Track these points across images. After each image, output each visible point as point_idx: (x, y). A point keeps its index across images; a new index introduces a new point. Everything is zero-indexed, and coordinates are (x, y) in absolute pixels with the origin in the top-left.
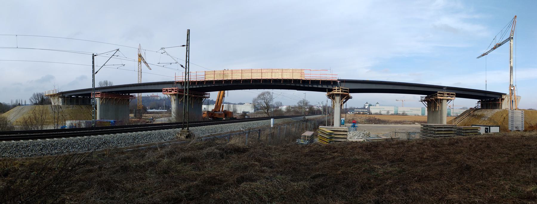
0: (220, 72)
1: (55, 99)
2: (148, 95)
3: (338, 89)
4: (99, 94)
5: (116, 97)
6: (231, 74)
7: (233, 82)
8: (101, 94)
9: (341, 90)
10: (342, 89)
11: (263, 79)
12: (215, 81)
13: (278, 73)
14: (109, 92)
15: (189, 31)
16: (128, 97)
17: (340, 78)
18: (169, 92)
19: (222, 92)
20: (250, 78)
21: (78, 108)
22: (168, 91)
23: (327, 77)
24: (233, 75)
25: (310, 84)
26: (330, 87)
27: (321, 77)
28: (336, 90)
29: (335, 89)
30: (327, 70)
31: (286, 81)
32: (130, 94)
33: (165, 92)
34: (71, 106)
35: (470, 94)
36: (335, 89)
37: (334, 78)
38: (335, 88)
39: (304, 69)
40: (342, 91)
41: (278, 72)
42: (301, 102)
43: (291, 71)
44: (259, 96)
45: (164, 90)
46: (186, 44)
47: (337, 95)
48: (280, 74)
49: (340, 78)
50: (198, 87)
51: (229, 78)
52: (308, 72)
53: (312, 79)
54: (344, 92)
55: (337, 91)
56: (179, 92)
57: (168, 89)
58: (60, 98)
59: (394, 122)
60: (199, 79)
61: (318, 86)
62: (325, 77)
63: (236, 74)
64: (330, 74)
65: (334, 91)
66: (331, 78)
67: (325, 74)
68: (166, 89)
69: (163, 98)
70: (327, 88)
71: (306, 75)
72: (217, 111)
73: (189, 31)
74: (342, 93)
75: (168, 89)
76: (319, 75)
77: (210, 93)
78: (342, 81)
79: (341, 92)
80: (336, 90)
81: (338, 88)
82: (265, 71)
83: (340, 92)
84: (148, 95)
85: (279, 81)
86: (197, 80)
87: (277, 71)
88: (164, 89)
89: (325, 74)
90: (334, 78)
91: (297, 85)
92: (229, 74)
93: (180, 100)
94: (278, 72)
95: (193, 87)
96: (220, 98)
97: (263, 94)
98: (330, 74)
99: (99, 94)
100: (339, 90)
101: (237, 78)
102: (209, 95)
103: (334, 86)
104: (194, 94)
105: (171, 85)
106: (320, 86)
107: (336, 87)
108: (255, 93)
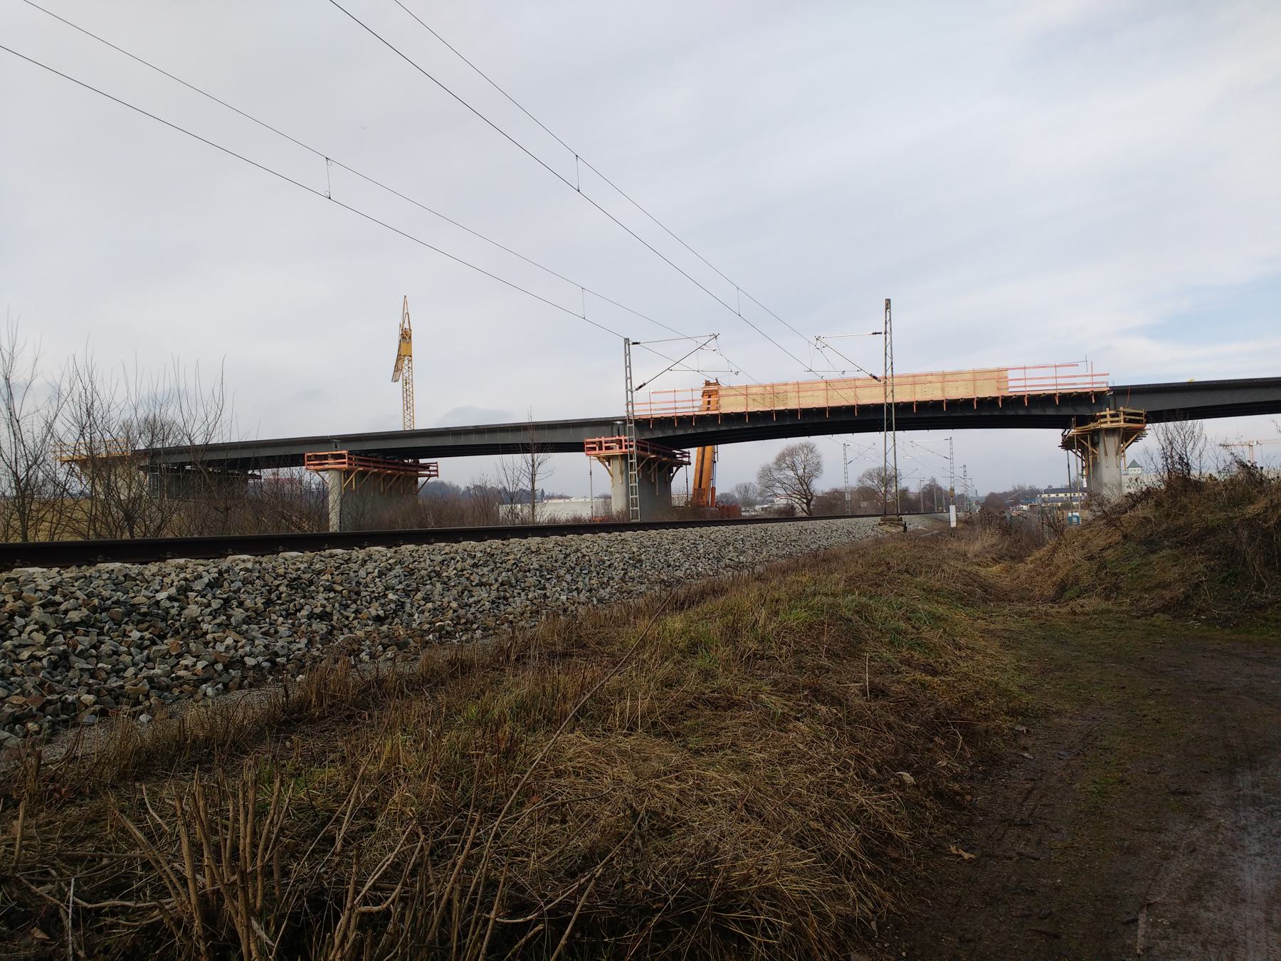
0: (760, 390)
3: (1112, 416)
9: (1122, 417)
10: (1125, 413)
11: (655, 418)
12: (750, 414)
13: (930, 385)
16: (415, 469)
19: (708, 448)
20: (852, 402)
22: (604, 445)
23: (1075, 384)
26: (1083, 411)
27: (1056, 385)
29: (1105, 416)
31: (953, 404)
32: (422, 461)
33: (594, 449)
36: (1105, 416)
37: (1095, 383)
38: (1102, 413)
40: (1125, 421)
41: (930, 382)
42: (870, 476)
43: (968, 376)
44: (781, 458)
45: (588, 443)
46: (631, 346)
47: (1111, 432)
48: (939, 385)
50: (681, 432)
51: (792, 405)
52: (1019, 374)
53: (1031, 393)
54: (1131, 421)
55: (1111, 422)
57: (603, 439)
59: (109, 774)
60: (1035, 382)
62: (1072, 384)
63: (809, 393)
64: (1086, 376)
65: (1102, 420)
66: (1088, 386)
67: (1072, 377)
68: (597, 439)
70: (1073, 416)
71: (1010, 384)
75: (603, 439)
76: (1052, 378)
78: (1121, 393)
79: (1122, 423)
80: (1109, 419)
81: (1112, 412)
83: (1122, 424)
85: (937, 405)
86: (654, 416)
87: (930, 378)
88: (588, 440)
89: (1072, 377)
90: (1095, 383)
92: (790, 395)
94: (930, 382)
96: (706, 465)
97: (792, 452)
98: (1086, 376)
99: (342, 456)
100: (1118, 416)
101: (812, 403)
105: (607, 429)
107: (1108, 409)
108: (768, 450)
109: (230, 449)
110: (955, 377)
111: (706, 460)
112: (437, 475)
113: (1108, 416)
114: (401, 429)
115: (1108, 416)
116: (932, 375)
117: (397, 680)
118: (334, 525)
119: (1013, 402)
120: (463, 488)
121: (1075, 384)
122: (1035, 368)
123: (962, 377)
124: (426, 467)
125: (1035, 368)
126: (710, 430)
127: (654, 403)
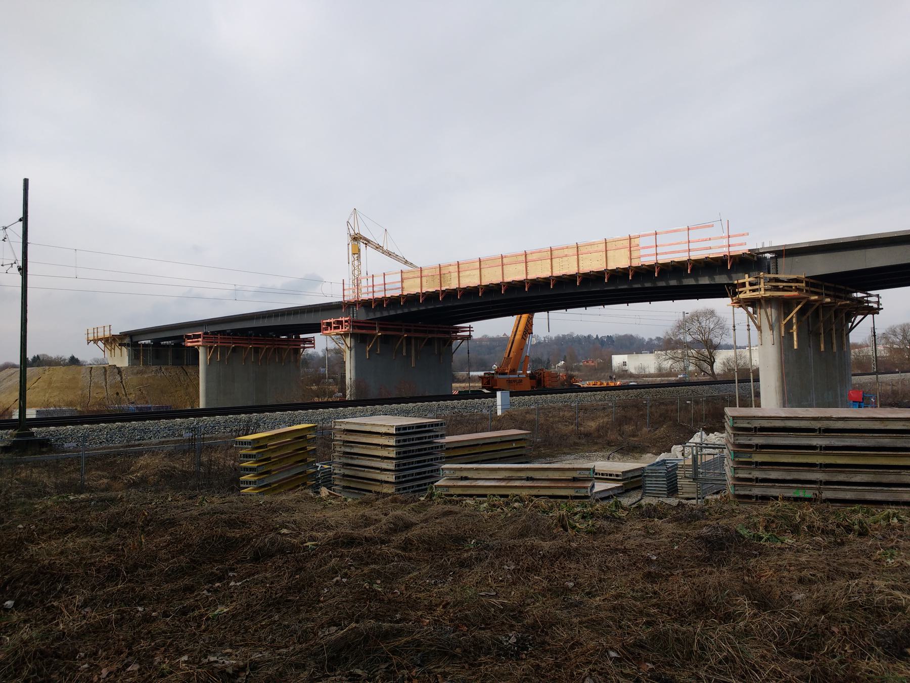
1: (114, 349)
2: (505, 334)
3: (751, 284)
4: (199, 336)
5: (251, 344)
6: (456, 274)
7: (463, 295)
8: (204, 338)
14: (235, 332)
15: (26, 182)
17: (770, 242)
18: (335, 328)
19: (525, 316)
21: (173, 374)
23: (710, 248)
24: (461, 275)
25: (688, 276)
28: (748, 287)
29: (743, 285)
30: (713, 226)
32: (302, 336)
34: (154, 368)
35: (274, 433)
36: (743, 285)
38: (741, 281)
39: (637, 234)
41: (566, 256)
49: (770, 242)
50: (406, 310)
56: (354, 327)
57: (332, 320)
58: (123, 347)
61: (697, 280)
63: (468, 273)
69: (545, 340)
71: (643, 252)
72: (506, 371)
73: (26, 182)
74: (768, 294)
77: (472, 324)
80: (748, 287)
81: (751, 279)
82: (535, 256)
83: (762, 293)
84: (505, 334)
91: (620, 287)
93: (368, 349)
94: (566, 256)
95: (382, 313)
99: (199, 336)
102: (470, 331)
103: (734, 276)
104: (407, 331)
106: (691, 282)
107: (747, 276)
109: (138, 335)
110: (589, 249)
111: (518, 333)
112: (314, 347)
113: (747, 284)
114: (340, 299)
115: (747, 284)
116: (567, 248)
117: (222, 629)
118: (202, 405)
119: (675, 269)
120: (647, 340)
121: (710, 248)
122: (667, 232)
123: (595, 248)
124: (305, 341)
125: (667, 232)
126: (430, 307)
127: (734, 245)
